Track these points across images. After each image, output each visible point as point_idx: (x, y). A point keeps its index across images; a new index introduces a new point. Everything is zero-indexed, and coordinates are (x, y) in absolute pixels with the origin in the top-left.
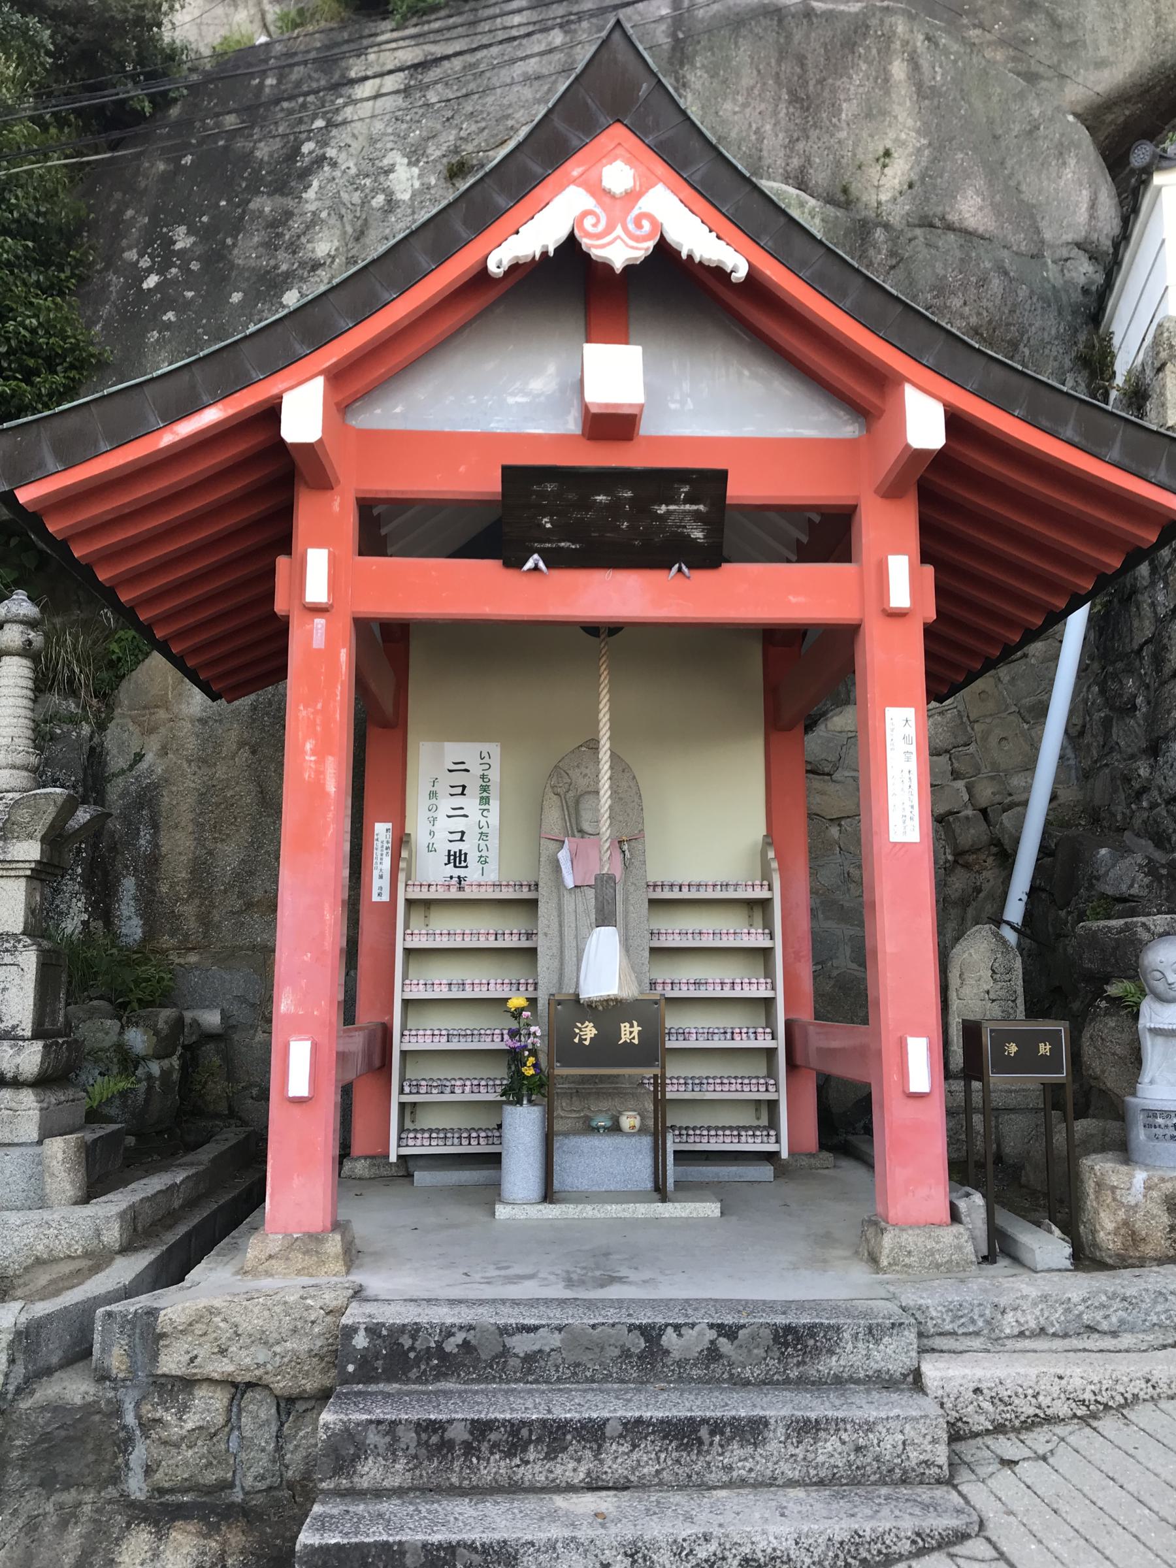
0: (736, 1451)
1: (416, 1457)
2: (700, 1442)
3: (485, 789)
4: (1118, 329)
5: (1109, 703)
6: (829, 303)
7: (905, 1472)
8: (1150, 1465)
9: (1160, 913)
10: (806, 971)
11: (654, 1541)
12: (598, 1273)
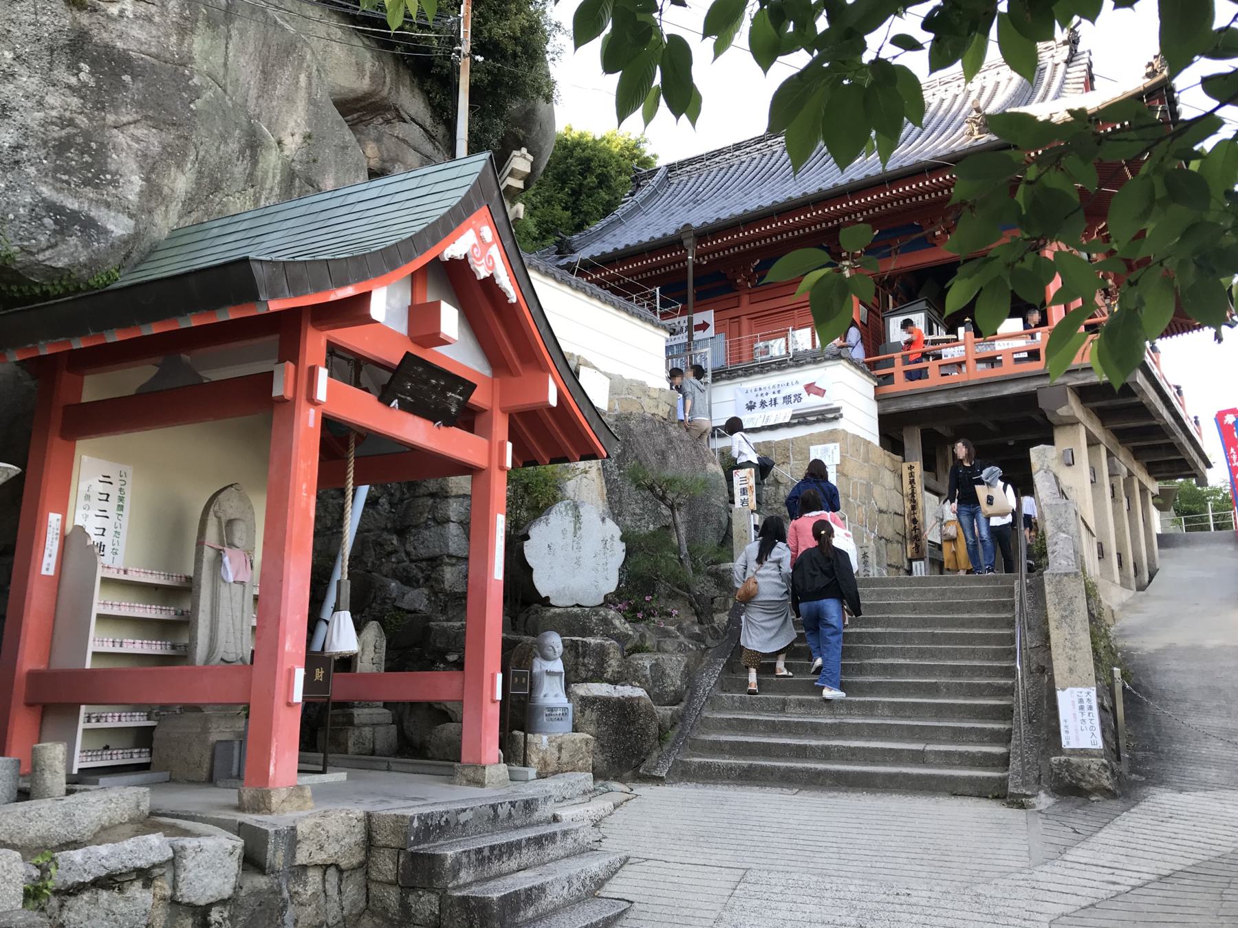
3: (121, 499)
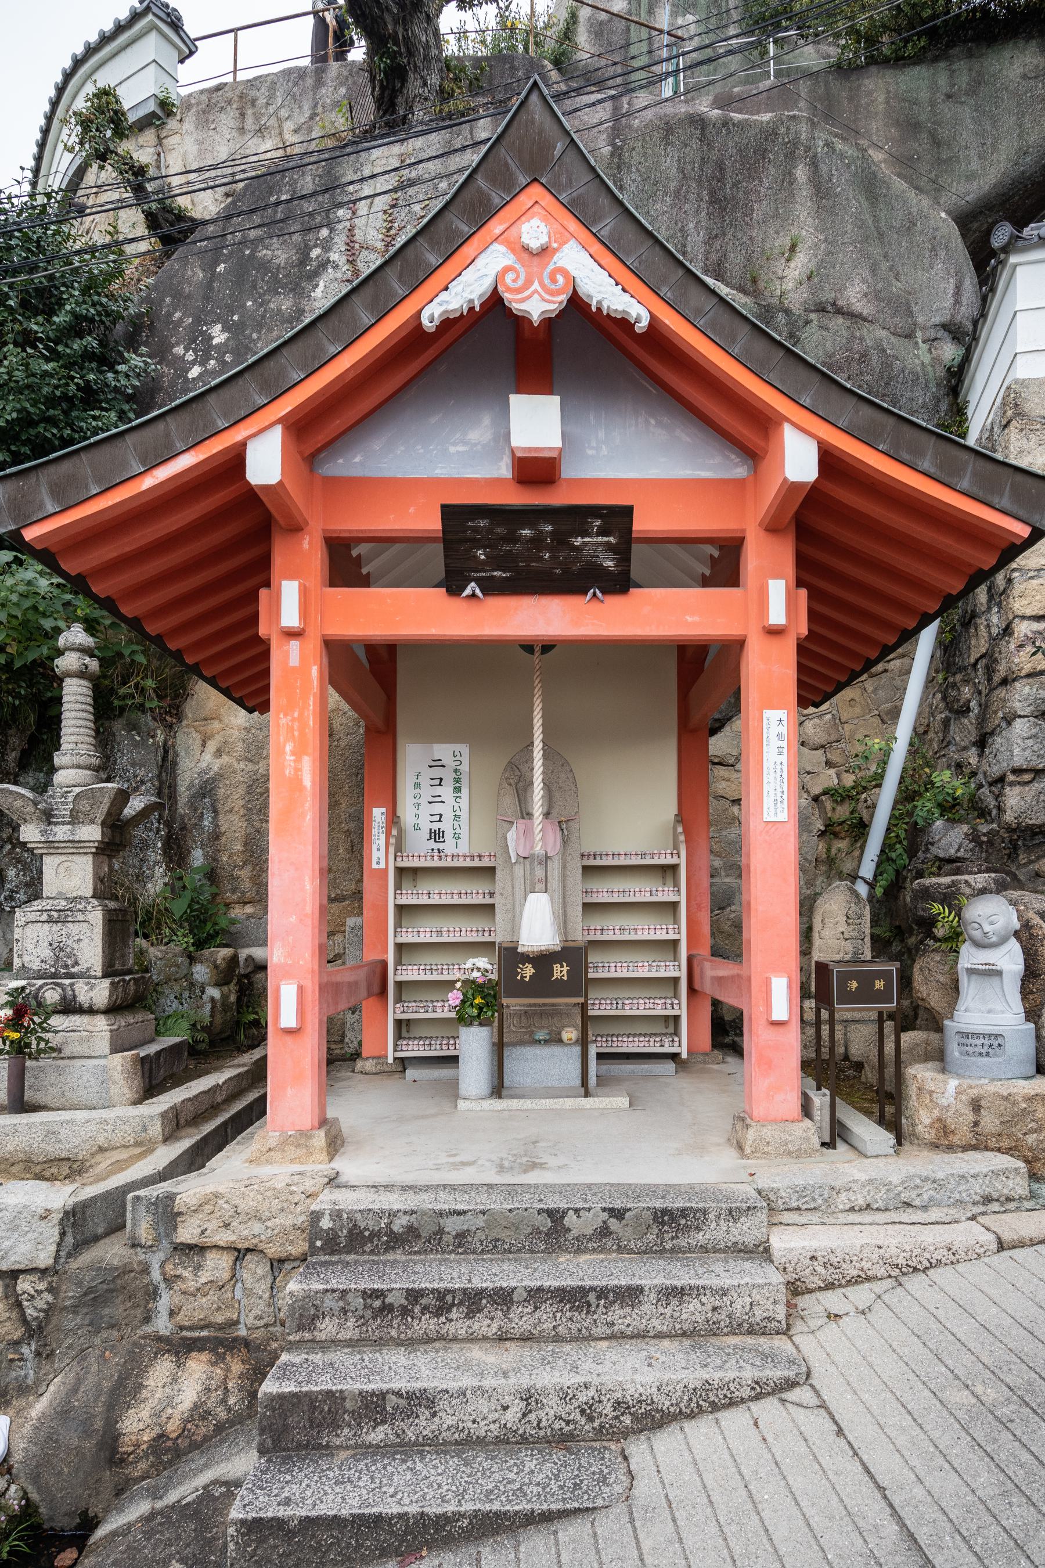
0: (616, 1313)
1: (363, 1317)
2: (589, 1305)
3: (457, 780)
4: (973, 398)
5: (949, 707)
6: (718, 349)
7: (751, 1325)
8: (947, 1325)
9: (979, 872)
10: (705, 918)
11: (544, 1389)
12: (525, 1159)
